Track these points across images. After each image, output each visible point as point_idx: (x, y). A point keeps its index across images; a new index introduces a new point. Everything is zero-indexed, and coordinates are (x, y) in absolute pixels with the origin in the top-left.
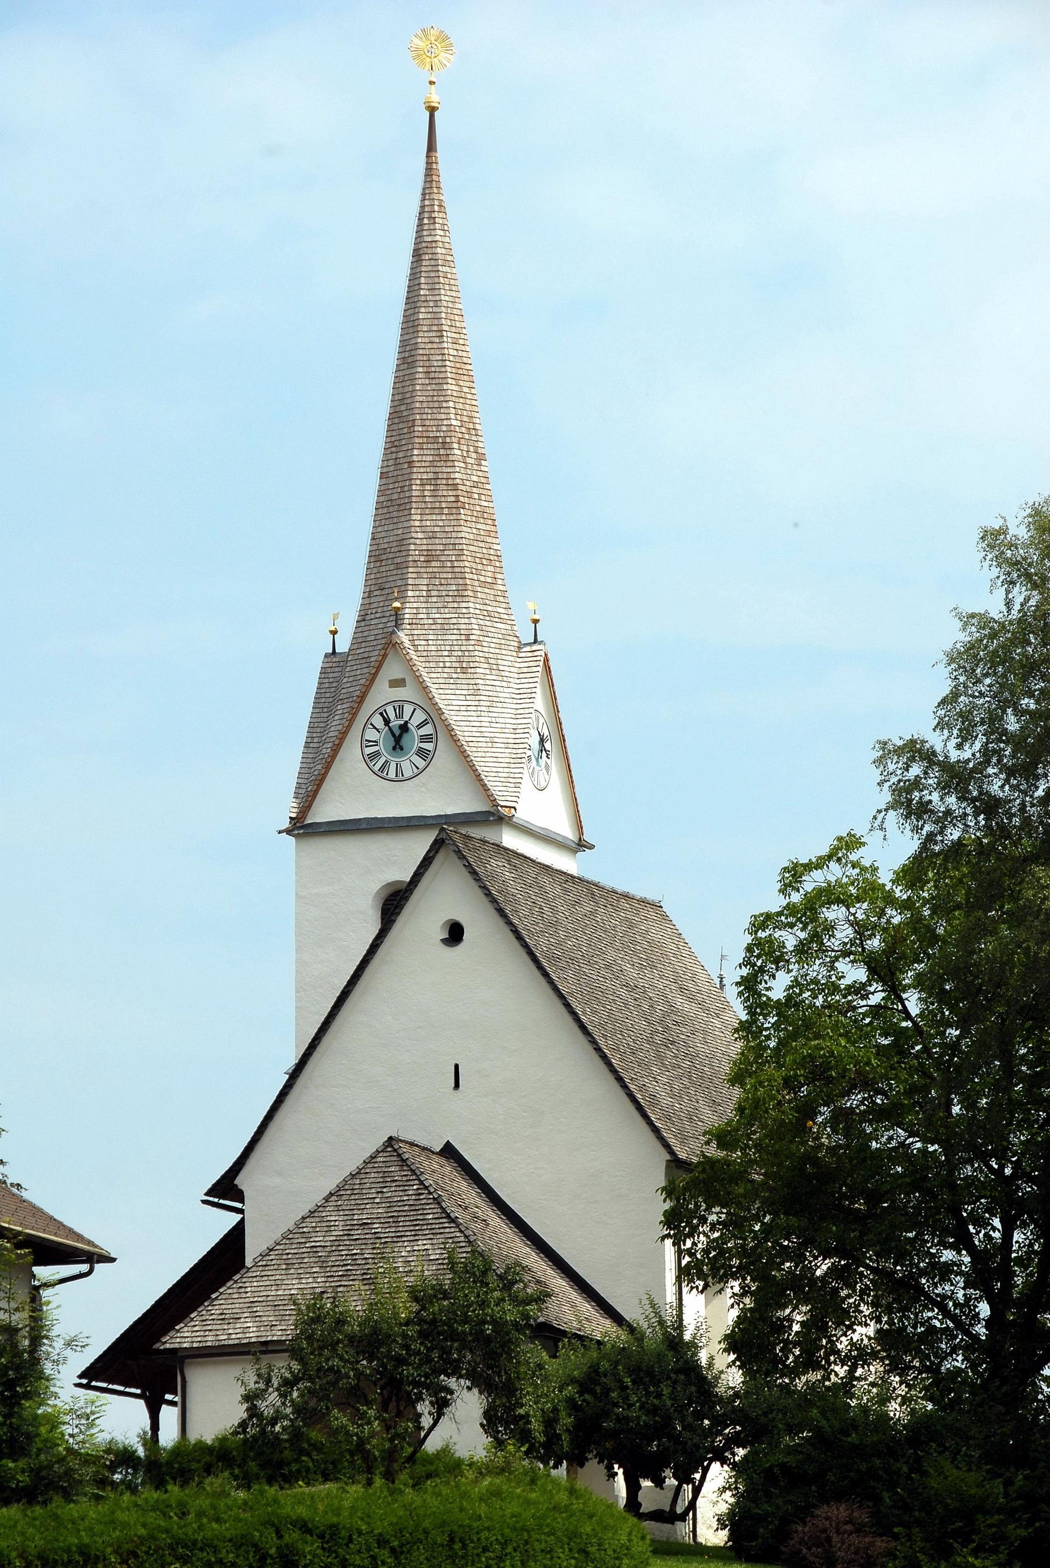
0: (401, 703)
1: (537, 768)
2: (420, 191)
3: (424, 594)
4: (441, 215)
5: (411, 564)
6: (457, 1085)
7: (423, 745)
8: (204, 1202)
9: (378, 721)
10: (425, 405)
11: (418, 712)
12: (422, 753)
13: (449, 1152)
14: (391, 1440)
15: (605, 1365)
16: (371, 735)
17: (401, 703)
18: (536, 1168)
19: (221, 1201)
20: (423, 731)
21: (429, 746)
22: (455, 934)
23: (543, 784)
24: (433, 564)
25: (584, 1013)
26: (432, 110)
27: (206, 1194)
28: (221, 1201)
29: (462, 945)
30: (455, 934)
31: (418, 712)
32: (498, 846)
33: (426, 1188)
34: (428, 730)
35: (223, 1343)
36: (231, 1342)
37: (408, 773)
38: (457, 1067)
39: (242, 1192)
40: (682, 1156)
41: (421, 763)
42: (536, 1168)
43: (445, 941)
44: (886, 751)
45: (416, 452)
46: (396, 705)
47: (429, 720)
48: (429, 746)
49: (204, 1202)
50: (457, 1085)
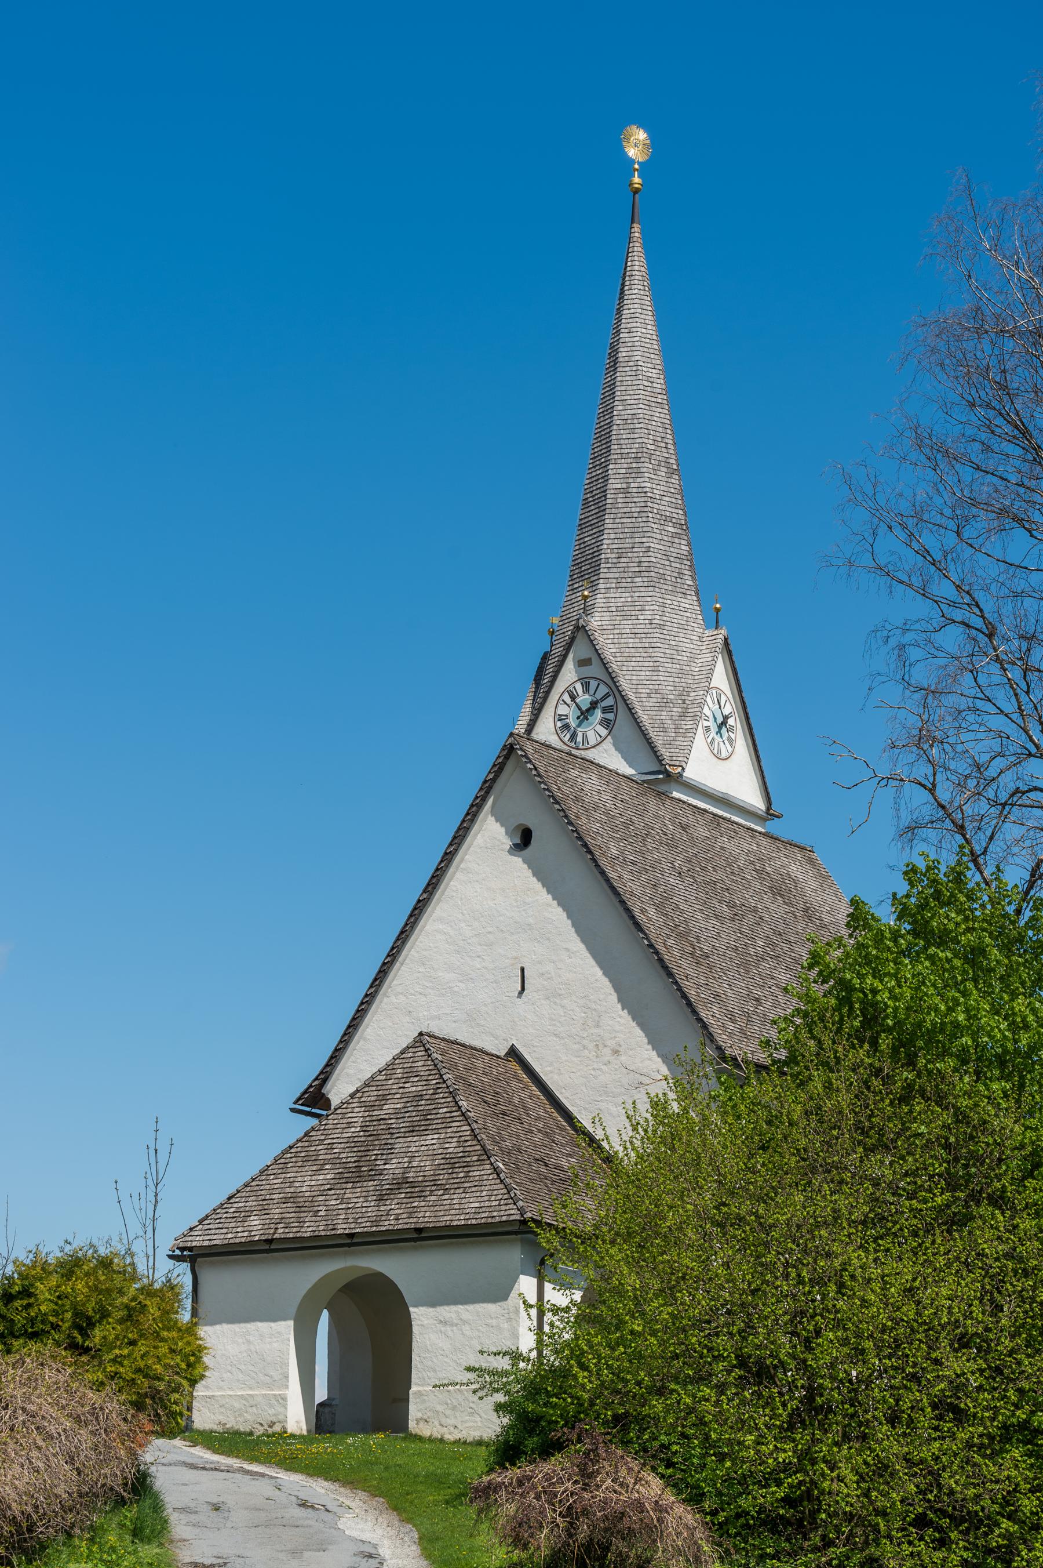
1: (718, 738)
5: (603, 561)
8: (292, 1110)
9: (567, 698)
10: (621, 427)
11: (602, 686)
13: (513, 1053)
15: (1000, 1314)
16: (563, 710)
18: (594, 1069)
21: (610, 716)
23: (724, 754)
25: (643, 911)
27: (295, 1103)
31: (602, 686)
33: (445, 1082)
34: (609, 702)
35: (231, 1241)
36: (237, 1241)
37: (592, 741)
38: (523, 970)
40: (734, 1048)
42: (594, 1069)
45: (611, 466)
48: (610, 716)
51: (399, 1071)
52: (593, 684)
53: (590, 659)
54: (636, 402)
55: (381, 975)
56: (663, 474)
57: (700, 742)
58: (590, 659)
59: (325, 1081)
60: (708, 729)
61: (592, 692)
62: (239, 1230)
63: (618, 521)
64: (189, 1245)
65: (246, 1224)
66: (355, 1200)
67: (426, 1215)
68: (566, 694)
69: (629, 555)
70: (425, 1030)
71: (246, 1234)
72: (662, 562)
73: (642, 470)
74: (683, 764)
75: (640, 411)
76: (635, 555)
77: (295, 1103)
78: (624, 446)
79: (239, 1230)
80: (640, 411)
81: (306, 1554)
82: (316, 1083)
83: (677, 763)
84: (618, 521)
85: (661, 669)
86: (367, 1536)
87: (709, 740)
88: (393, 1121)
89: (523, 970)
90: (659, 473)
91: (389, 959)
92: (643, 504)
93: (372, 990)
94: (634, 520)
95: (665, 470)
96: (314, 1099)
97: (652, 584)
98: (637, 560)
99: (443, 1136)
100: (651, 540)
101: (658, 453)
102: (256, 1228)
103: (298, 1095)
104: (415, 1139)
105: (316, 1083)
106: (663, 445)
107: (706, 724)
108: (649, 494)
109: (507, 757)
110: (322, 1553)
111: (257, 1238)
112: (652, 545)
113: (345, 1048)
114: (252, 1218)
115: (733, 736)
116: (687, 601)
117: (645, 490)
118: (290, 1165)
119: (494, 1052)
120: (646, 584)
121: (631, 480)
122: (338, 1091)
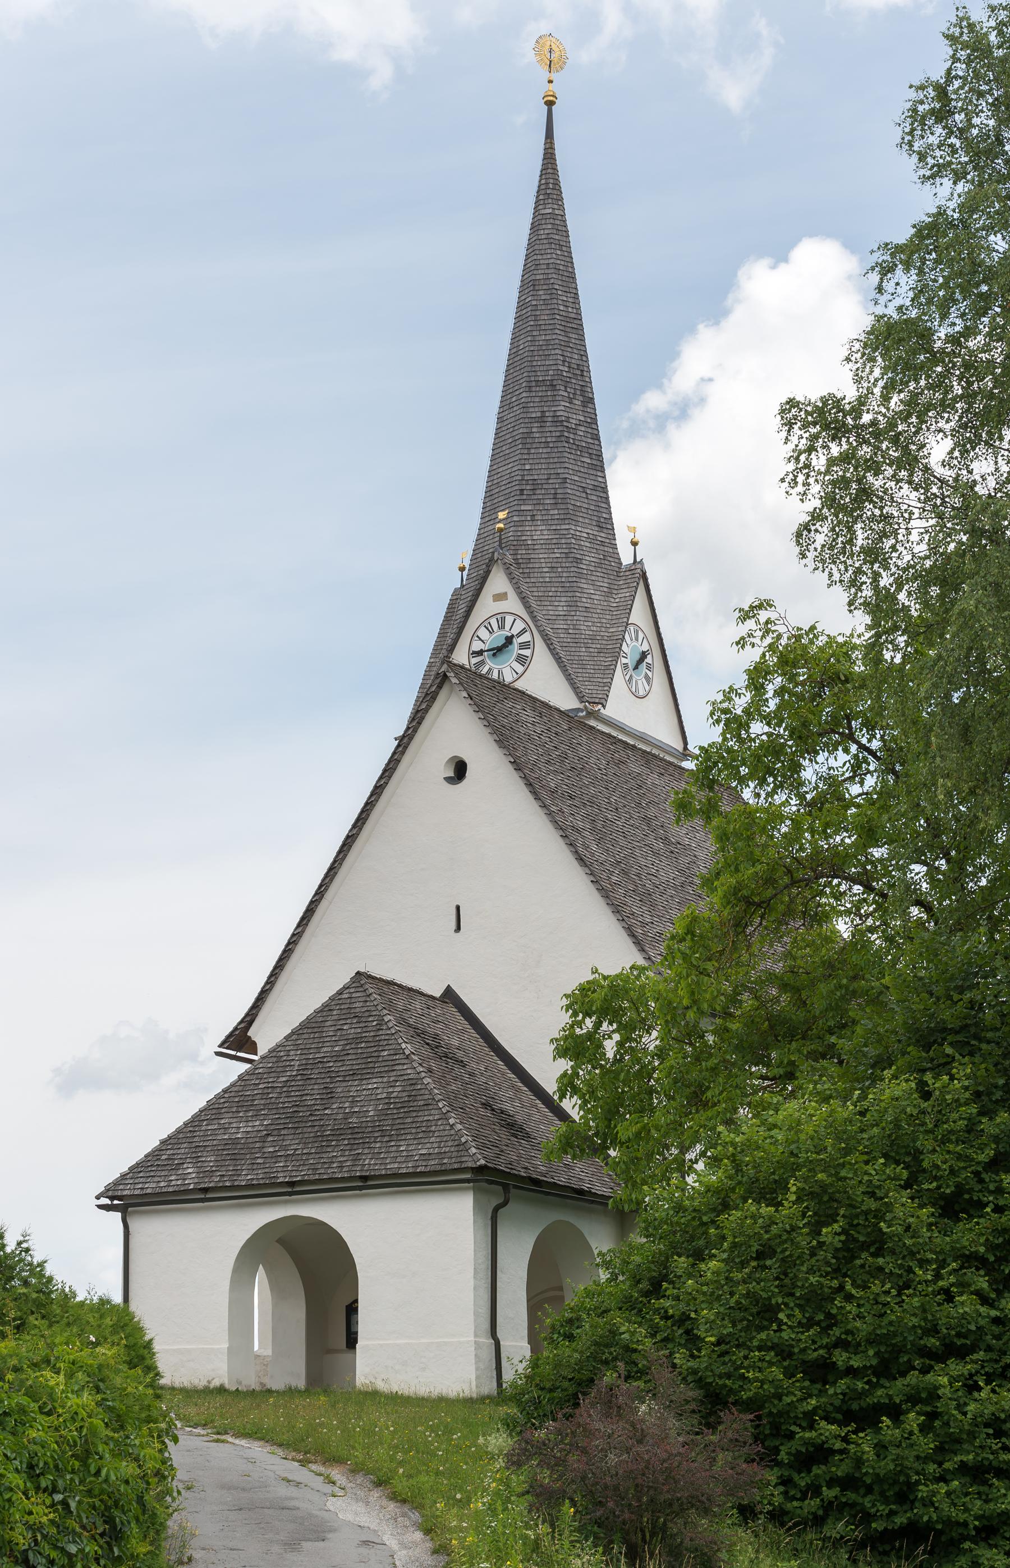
0: (502, 615)
2: (539, 173)
3: (529, 518)
4: (555, 192)
6: (458, 928)
7: (522, 652)
8: (218, 1054)
12: (521, 659)
13: (450, 995)
14: (830, 1348)
17: (502, 615)
19: (239, 1054)
20: (523, 639)
21: (527, 652)
22: (460, 770)
23: (642, 693)
24: (538, 492)
25: (587, 847)
26: (550, 104)
27: (220, 1046)
28: (239, 1054)
29: (465, 782)
30: (460, 770)
32: (524, 693)
36: (171, 1189)
38: (458, 908)
39: (254, 1044)
41: (520, 669)
43: (449, 780)
44: (790, 411)
46: (499, 616)
47: (527, 628)
48: (527, 652)
49: (218, 1054)
50: (458, 928)
51: (335, 1013)
52: (509, 620)
53: (506, 593)
54: (551, 327)
55: (309, 914)
56: (579, 403)
57: (619, 679)
58: (506, 593)
59: (250, 1023)
60: (626, 666)
61: (507, 628)
62: (173, 1178)
63: (533, 451)
64: (119, 1193)
65: (180, 1172)
66: (295, 1147)
67: (369, 1164)
68: (483, 628)
69: (545, 486)
70: (363, 970)
71: (179, 1182)
72: (578, 494)
73: (557, 398)
74: (603, 701)
75: (554, 337)
76: (551, 486)
77: (220, 1046)
78: (539, 374)
79: (173, 1178)
80: (554, 337)
81: (306, 1545)
82: (242, 1025)
83: (597, 700)
84: (533, 451)
85: (579, 604)
86: (364, 1520)
87: (627, 678)
88: (331, 1064)
89: (458, 908)
90: (551, 414)
91: (317, 898)
92: (558, 434)
93: (299, 930)
94: (549, 450)
95: (581, 398)
96: (239, 1041)
97: (568, 516)
98: (553, 491)
99: (385, 1080)
100: (566, 471)
101: (574, 381)
102: (190, 1175)
103: (223, 1038)
104: (356, 1083)
105: (242, 1025)
106: (579, 372)
107: (624, 661)
108: (565, 424)
109: (440, 687)
110: (321, 1544)
111: (192, 1187)
112: (567, 476)
113: (270, 989)
114: (185, 1166)
115: (650, 674)
116: (603, 535)
117: (560, 419)
118: (223, 1111)
119: (430, 993)
120: (562, 517)
121: (545, 409)
122: (267, 1036)
